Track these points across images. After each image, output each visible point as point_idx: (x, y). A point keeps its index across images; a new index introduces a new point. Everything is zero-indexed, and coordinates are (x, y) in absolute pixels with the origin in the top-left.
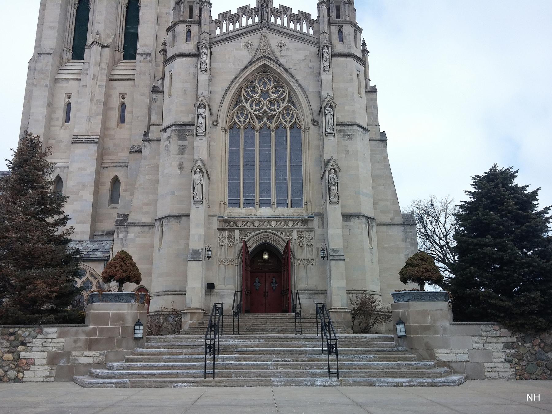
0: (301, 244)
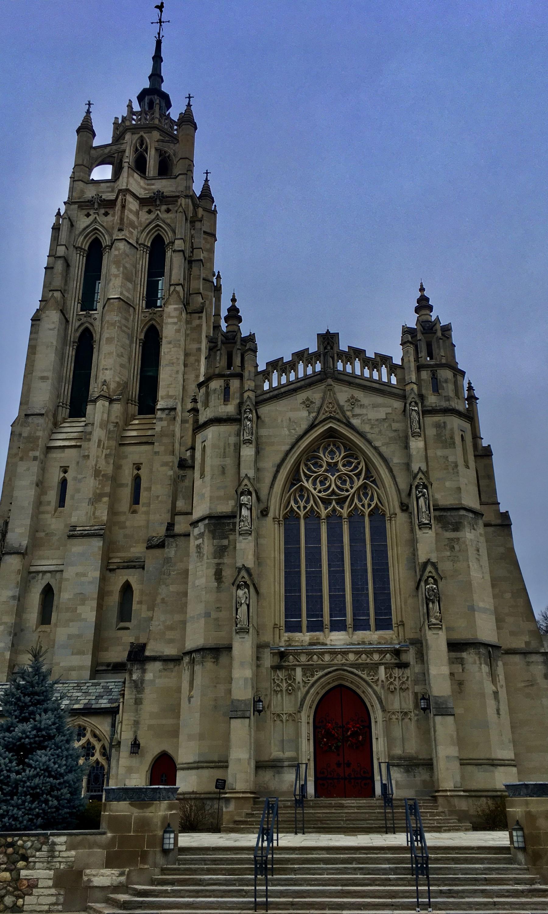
0: (392, 687)
